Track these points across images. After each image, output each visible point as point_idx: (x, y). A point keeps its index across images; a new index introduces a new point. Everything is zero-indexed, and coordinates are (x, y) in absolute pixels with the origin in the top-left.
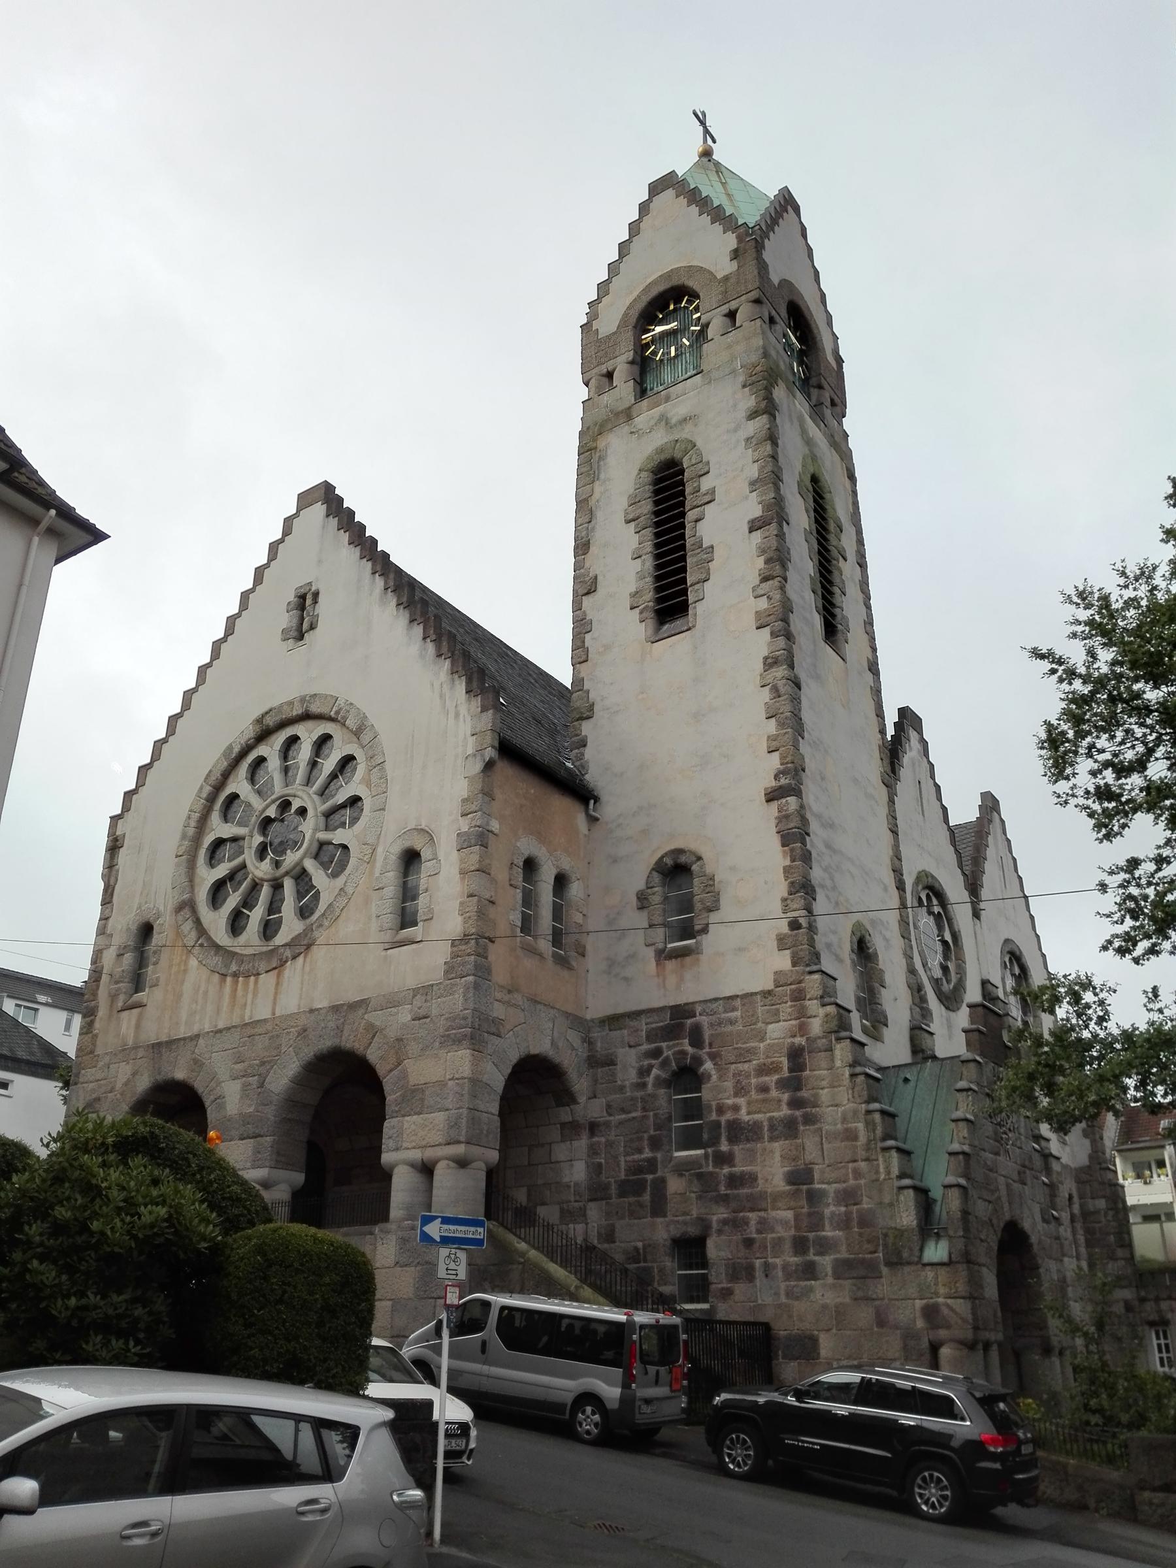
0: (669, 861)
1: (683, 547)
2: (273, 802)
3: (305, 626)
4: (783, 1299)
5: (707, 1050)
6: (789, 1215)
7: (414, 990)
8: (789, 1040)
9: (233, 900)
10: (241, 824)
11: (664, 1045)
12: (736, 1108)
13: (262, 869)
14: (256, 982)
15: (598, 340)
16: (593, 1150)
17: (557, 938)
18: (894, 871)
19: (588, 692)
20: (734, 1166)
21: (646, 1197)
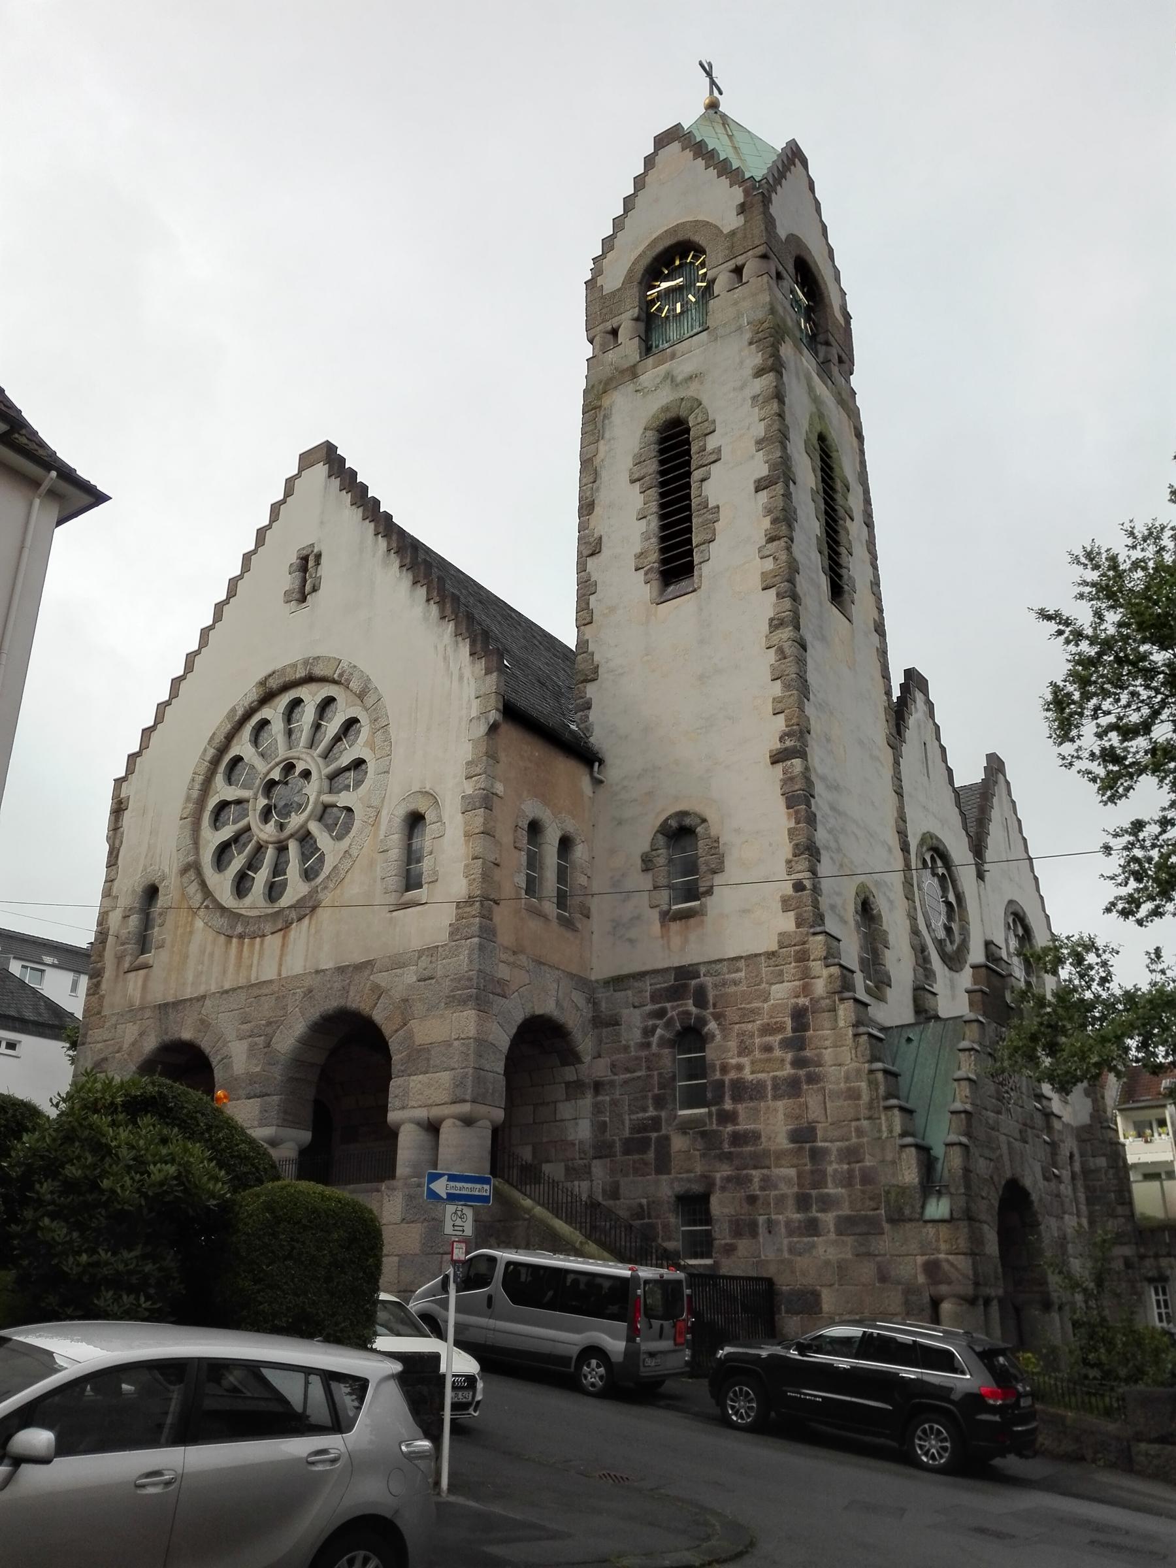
0: (673, 823)
1: (689, 507)
2: (277, 764)
3: (308, 588)
4: (786, 1255)
5: (711, 1010)
6: (792, 1172)
8: (793, 1001)
9: (237, 862)
11: (668, 1005)
12: (740, 1067)
13: (266, 832)
14: (262, 943)
15: (603, 297)
16: (598, 1109)
17: (562, 900)
18: (898, 832)
19: (592, 654)
20: (737, 1124)
21: (651, 1155)
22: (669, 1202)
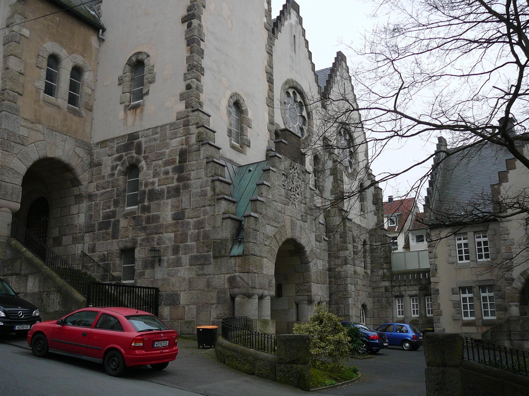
0: (134, 59)
5: (143, 155)
6: (172, 235)
8: (180, 147)
11: (124, 154)
16: (90, 208)
17: (73, 100)
18: (267, 73)
20: (150, 212)
21: (110, 230)
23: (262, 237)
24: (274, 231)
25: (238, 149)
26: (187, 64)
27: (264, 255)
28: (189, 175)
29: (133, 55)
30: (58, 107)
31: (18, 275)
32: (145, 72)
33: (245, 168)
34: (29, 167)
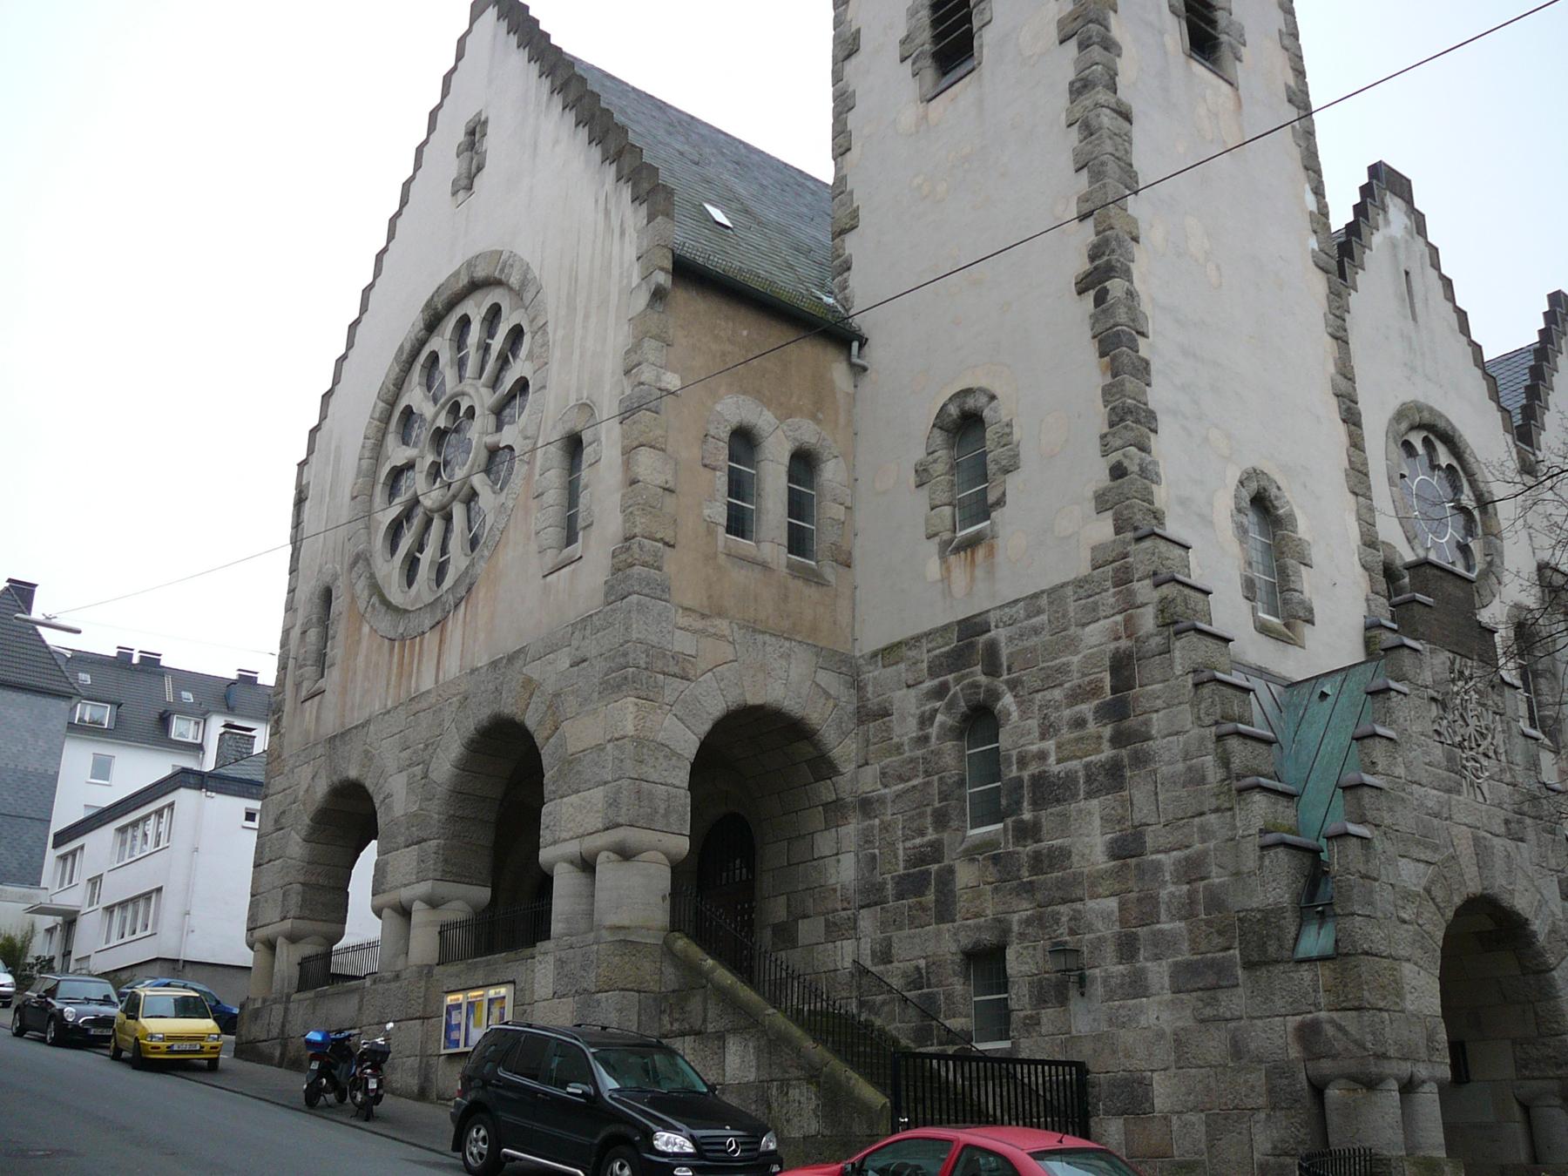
0: (953, 410)
5: (1005, 677)
6: (1113, 903)
7: (572, 625)
8: (1112, 646)
10: (415, 445)
11: (950, 677)
16: (866, 838)
17: (798, 542)
20: (1040, 841)
21: (930, 897)
22: (953, 962)
23: (1391, 898)
24: (1425, 875)
25: (1279, 633)
26: (1106, 406)
27: (1403, 952)
28: (1147, 723)
29: (950, 399)
30: (765, 566)
31: (698, 1033)
32: (988, 443)
33: (1305, 690)
34: (703, 738)
